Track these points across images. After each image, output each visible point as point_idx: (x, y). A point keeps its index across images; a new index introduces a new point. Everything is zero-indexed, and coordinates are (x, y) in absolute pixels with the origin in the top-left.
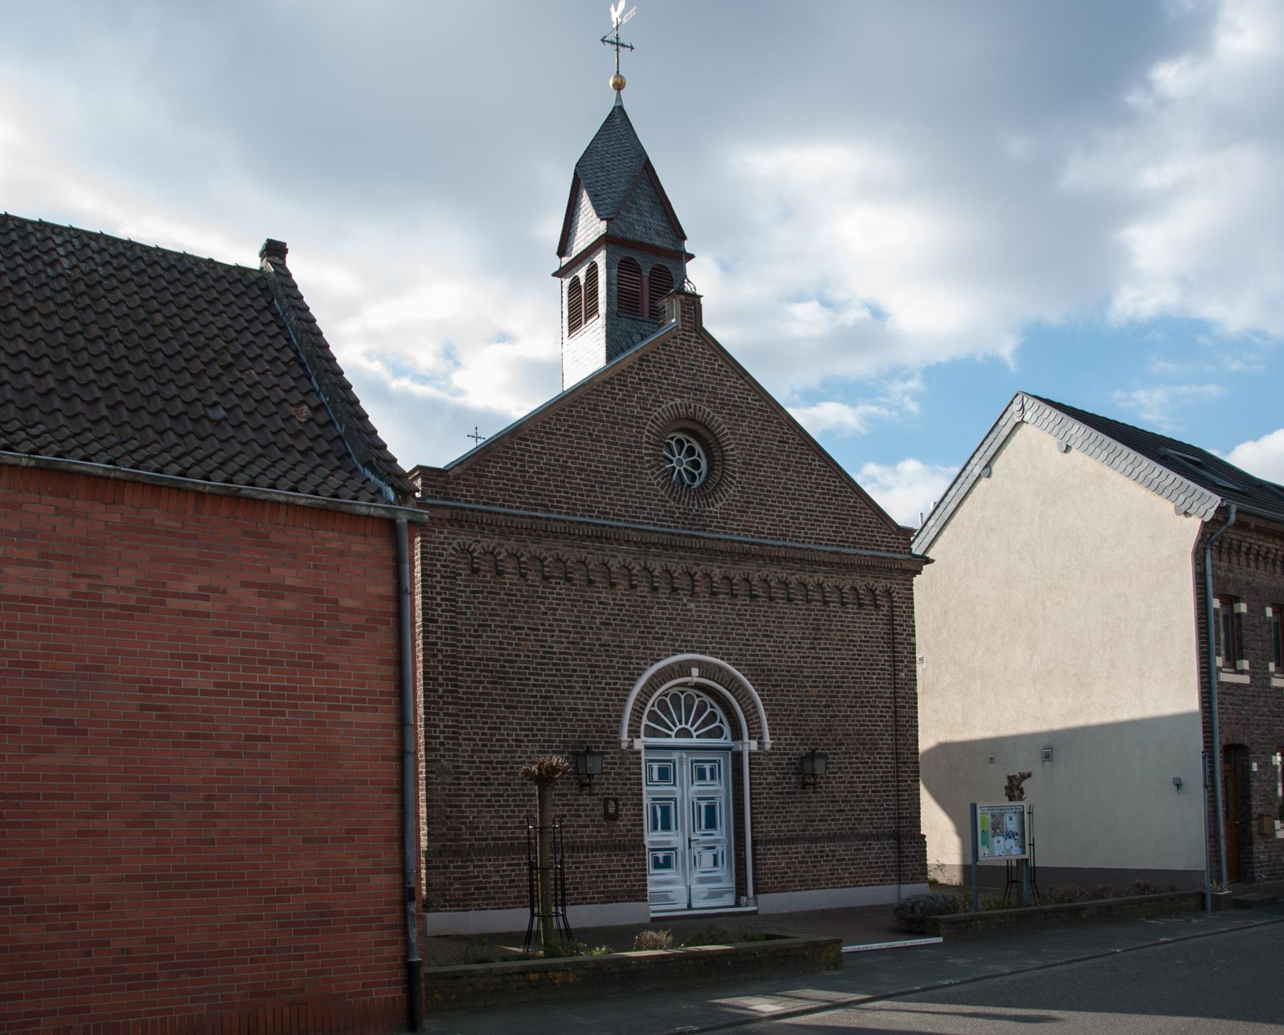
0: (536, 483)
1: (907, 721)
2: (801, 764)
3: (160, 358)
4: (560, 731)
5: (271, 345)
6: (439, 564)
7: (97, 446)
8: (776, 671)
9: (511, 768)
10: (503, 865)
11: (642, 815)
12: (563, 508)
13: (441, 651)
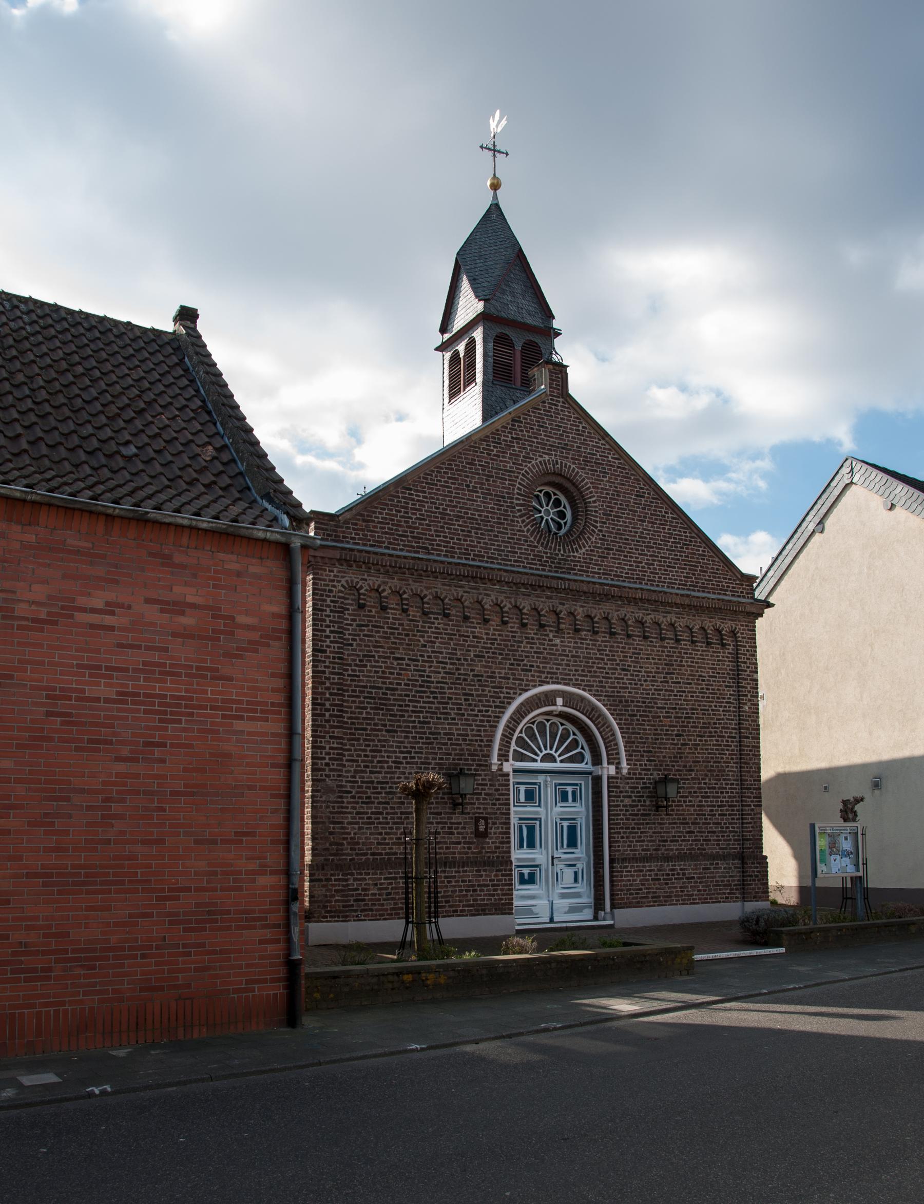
0: (418, 528)
1: (751, 751)
2: (655, 788)
3: (79, 402)
4: (436, 754)
5: (181, 395)
6: (329, 599)
7: (16, 473)
8: (632, 702)
9: (390, 788)
10: (380, 879)
11: (509, 833)
12: (442, 551)
13: (329, 679)
